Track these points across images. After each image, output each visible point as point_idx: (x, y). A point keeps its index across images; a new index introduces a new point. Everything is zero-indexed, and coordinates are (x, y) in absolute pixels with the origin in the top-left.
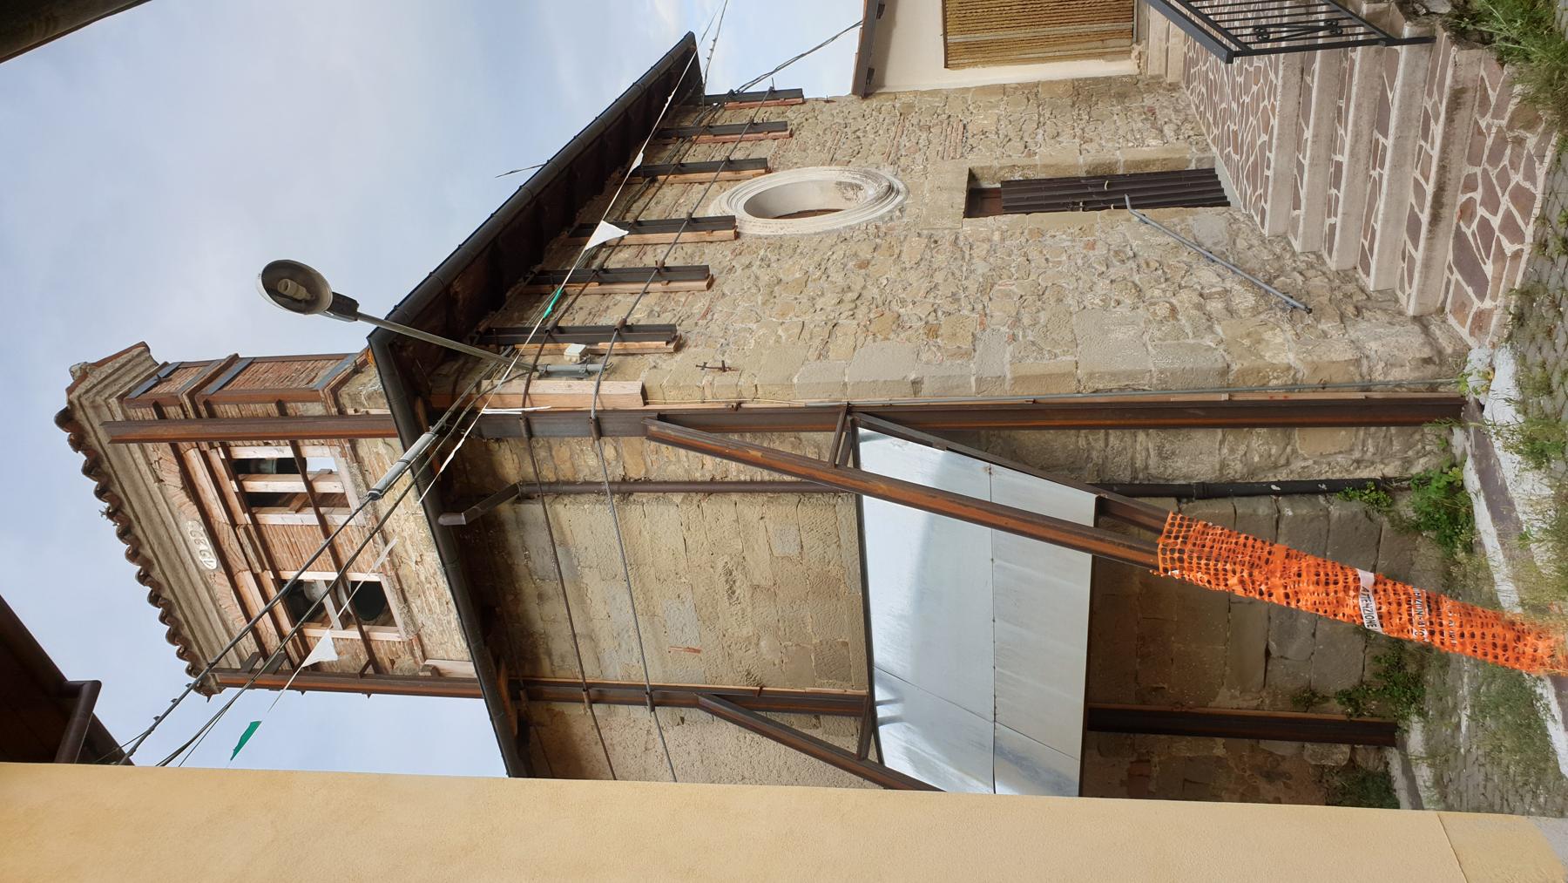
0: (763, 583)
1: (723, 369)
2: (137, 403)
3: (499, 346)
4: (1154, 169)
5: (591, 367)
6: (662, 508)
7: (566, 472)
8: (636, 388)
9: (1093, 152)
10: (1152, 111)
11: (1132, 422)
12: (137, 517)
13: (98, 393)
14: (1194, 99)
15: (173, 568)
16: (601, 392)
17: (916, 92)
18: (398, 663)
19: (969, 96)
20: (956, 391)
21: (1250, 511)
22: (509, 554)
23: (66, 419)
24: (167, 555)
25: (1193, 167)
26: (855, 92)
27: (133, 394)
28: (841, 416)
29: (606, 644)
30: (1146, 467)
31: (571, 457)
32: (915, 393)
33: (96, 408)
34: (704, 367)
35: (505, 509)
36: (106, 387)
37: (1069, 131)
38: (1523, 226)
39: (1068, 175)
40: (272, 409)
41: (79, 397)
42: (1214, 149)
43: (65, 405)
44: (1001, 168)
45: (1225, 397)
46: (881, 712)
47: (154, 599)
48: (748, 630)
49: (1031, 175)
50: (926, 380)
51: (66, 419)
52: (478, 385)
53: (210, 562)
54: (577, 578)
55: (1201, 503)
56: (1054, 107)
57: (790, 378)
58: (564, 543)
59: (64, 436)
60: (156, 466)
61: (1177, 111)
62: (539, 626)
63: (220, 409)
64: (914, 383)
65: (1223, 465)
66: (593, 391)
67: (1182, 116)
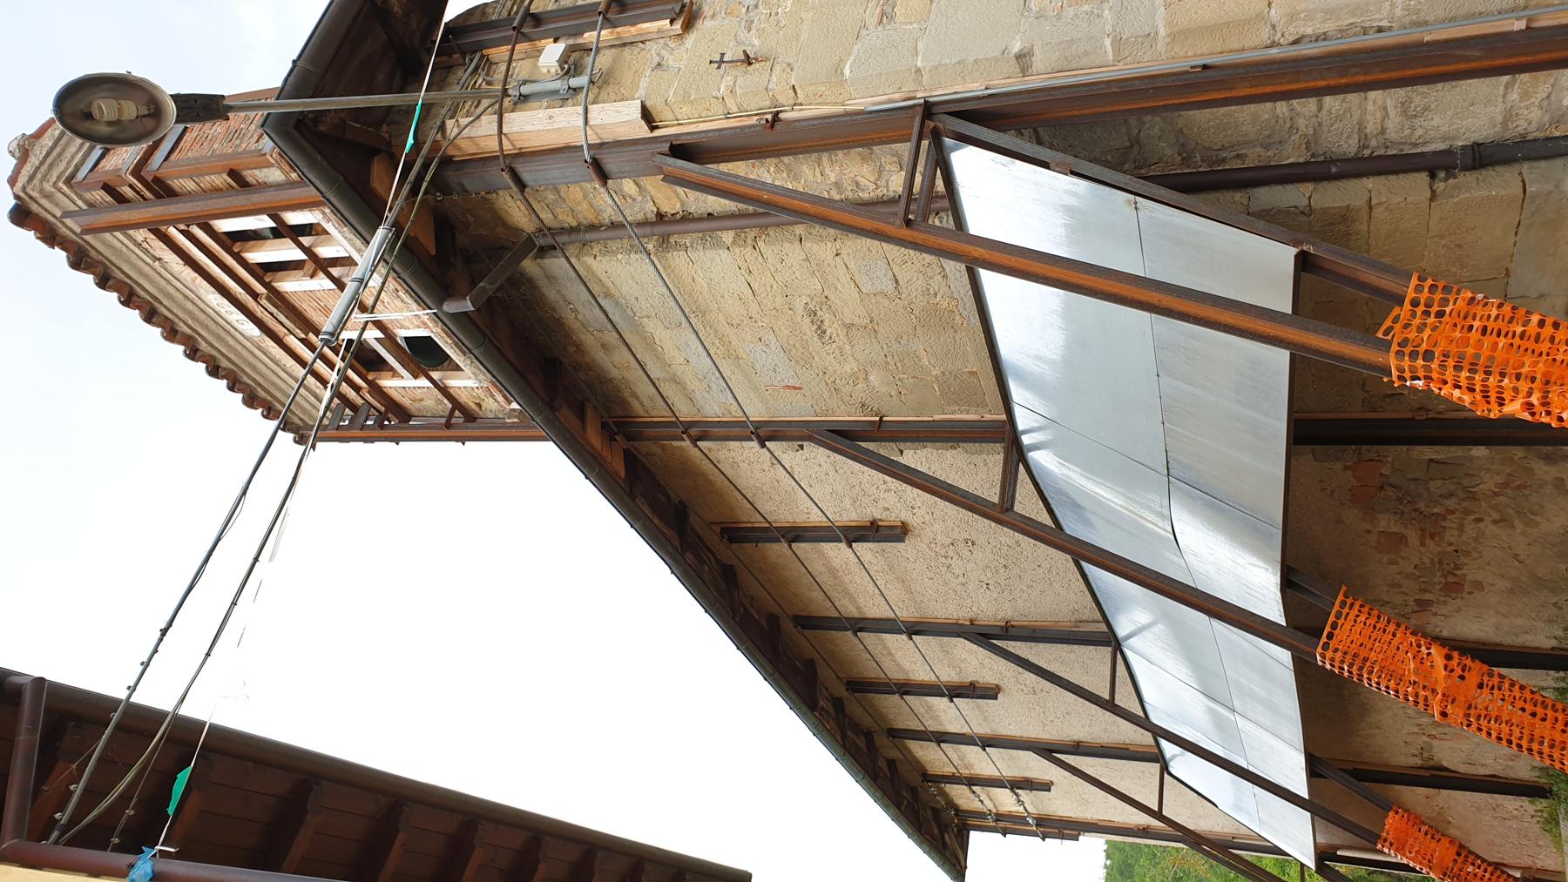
0: (857, 321)
1: (748, 60)
2: (86, 185)
3: (464, 55)
5: (574, 82)
6: (710, 253)
7: (587, 216)
8: (632, 110)
11: (1361, 78)
12: (156, 299)
13: (44, 177)
15: (220, 338)
16: (591, 122)
18: (484, 405)
20: (1085, 61)
21: (1549, 187)
22: (554, 309)
23: (22, 215)
24: (206, 327)
27: (81, 175)
28: (918, 120)
29: (694, 385)
30: (1383, 131)
31: (585, 196)
32: (1024, 71)
33: (48, 196)
34: (722, 61)
35: (529, 265)
36: (51, 166)
40: (221, 180)
41: (24, 189)
43: (13, 202)
45: (1520, 25)
46: (1026, 440)
47: (214, 371)
48: (850, 367)
50: (1037, 50)
51: (22, 215)
52: (442, 128)
53: (252, 330)
54: (638, 329)
55: (1468, 178)
57: (838, 70)
58: (608, 295)
59: (29, 236)
60: (145, 245)
62: (615, 373)
63: (176, 184)
64: (1020, 57)
65: (1509, 116)
66: (581, 122)
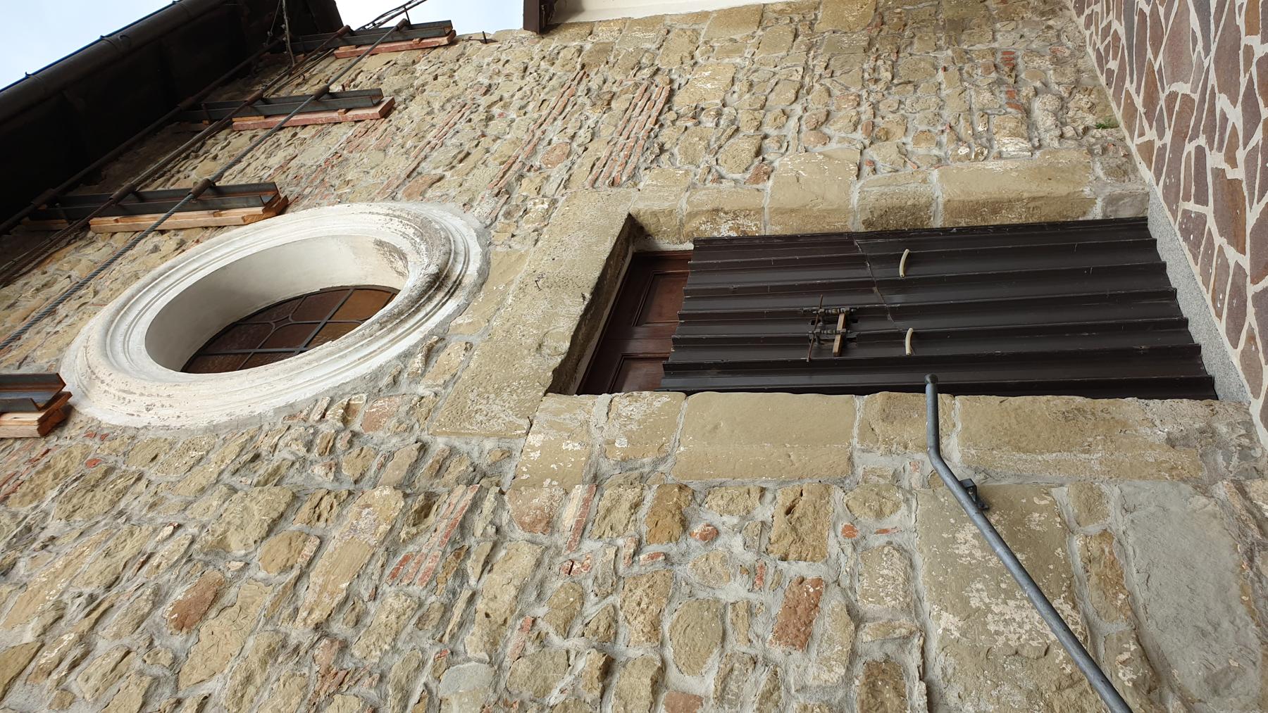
4: (1011, 218)
9: (884, 169)
10: (1010, 61)
14: (1094, 41)
17: (624, 20)
19: (704, 28)
25: (1096, 213)
26: (526, 27)
37: (847, 111)
38: (1212, 66)
39: (827, 228)
42: (1147, 174)
44: (692, 216)
49: (753, 228)
56: (836, 50)
61: (1058, 62)
67: (1070, 75)
